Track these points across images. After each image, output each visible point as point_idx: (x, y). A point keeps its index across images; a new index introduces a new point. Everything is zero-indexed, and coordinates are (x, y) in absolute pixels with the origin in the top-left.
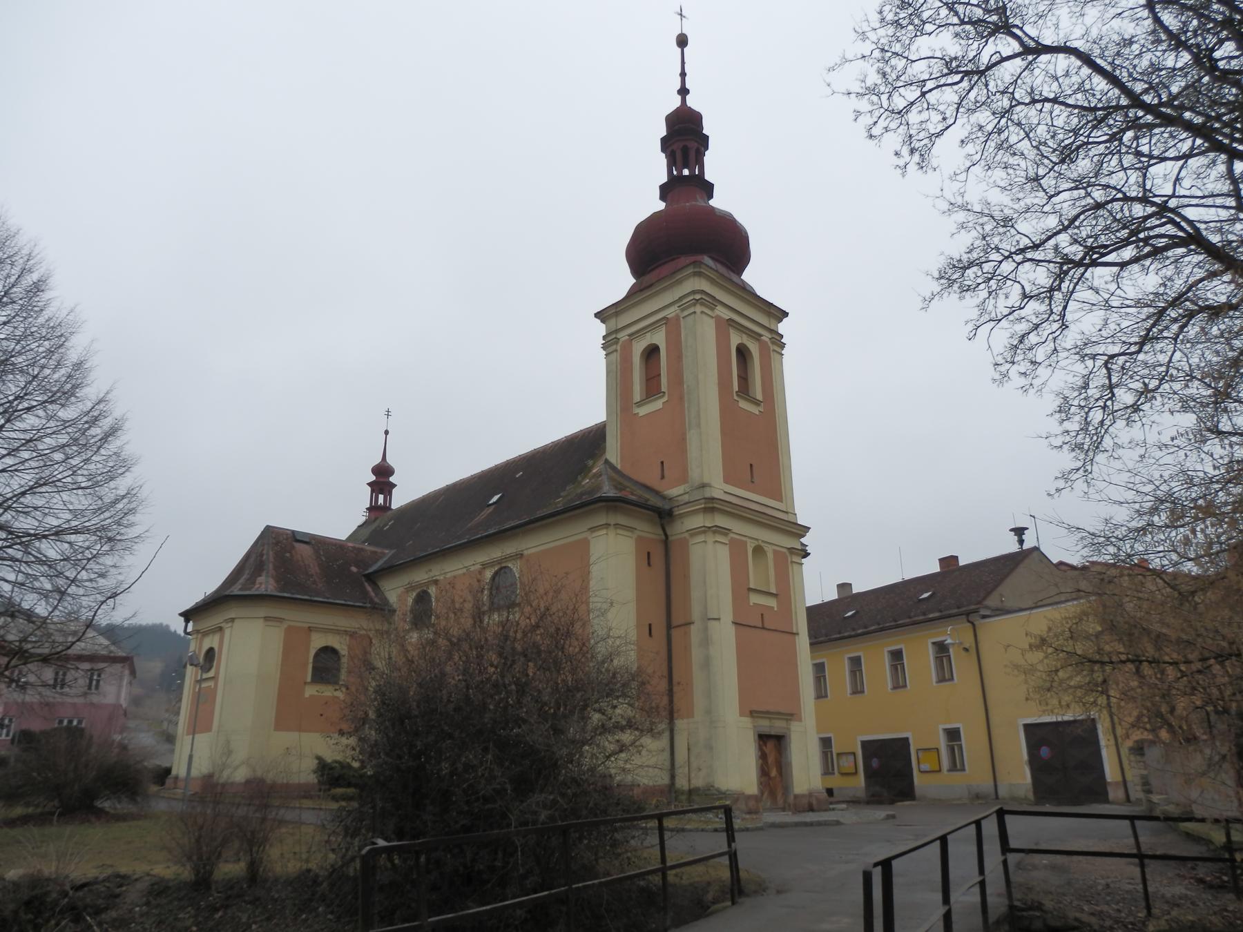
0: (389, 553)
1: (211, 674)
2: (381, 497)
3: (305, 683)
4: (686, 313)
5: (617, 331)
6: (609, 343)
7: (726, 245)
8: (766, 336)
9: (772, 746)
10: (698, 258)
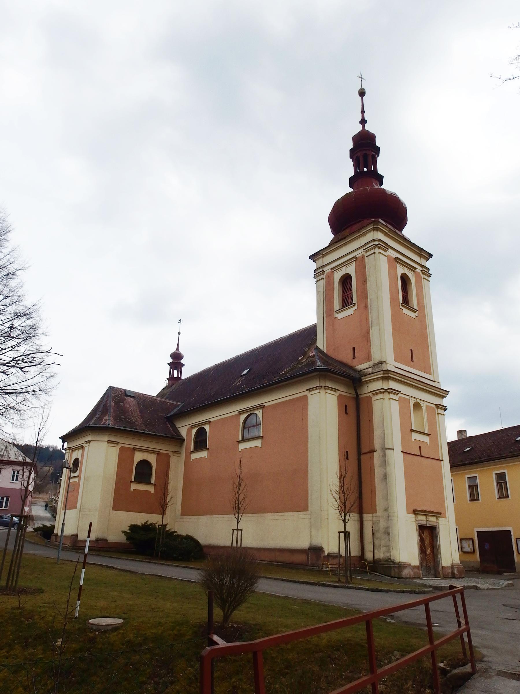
0: (180, 405)
1: (77, 474)
2: (176, 372)
3: (131, 482)
4: (369, 253)
5: (323, 267)
6: (318, 273)
7: (392, 213)
8: (419, 269)
9: (428, 535)
10: (377, 220)
